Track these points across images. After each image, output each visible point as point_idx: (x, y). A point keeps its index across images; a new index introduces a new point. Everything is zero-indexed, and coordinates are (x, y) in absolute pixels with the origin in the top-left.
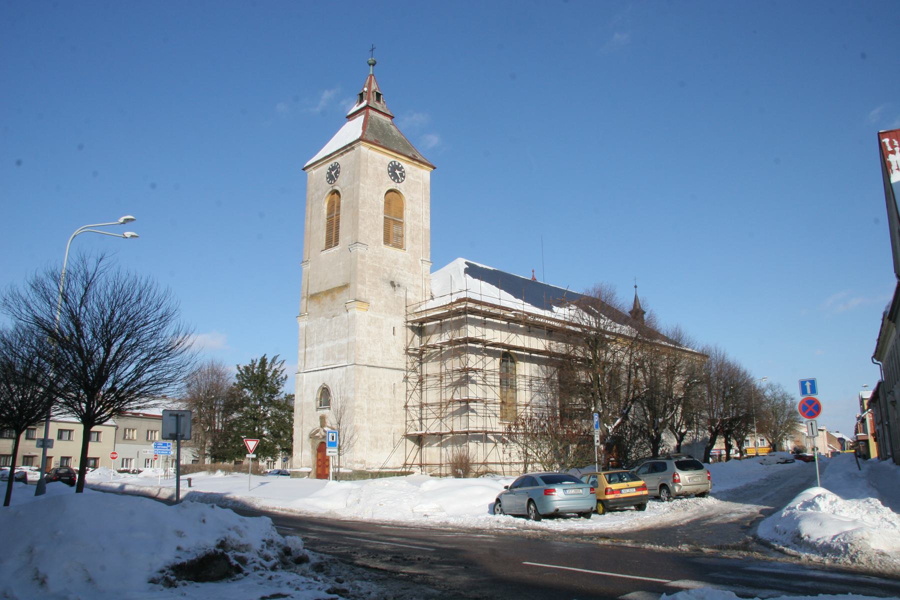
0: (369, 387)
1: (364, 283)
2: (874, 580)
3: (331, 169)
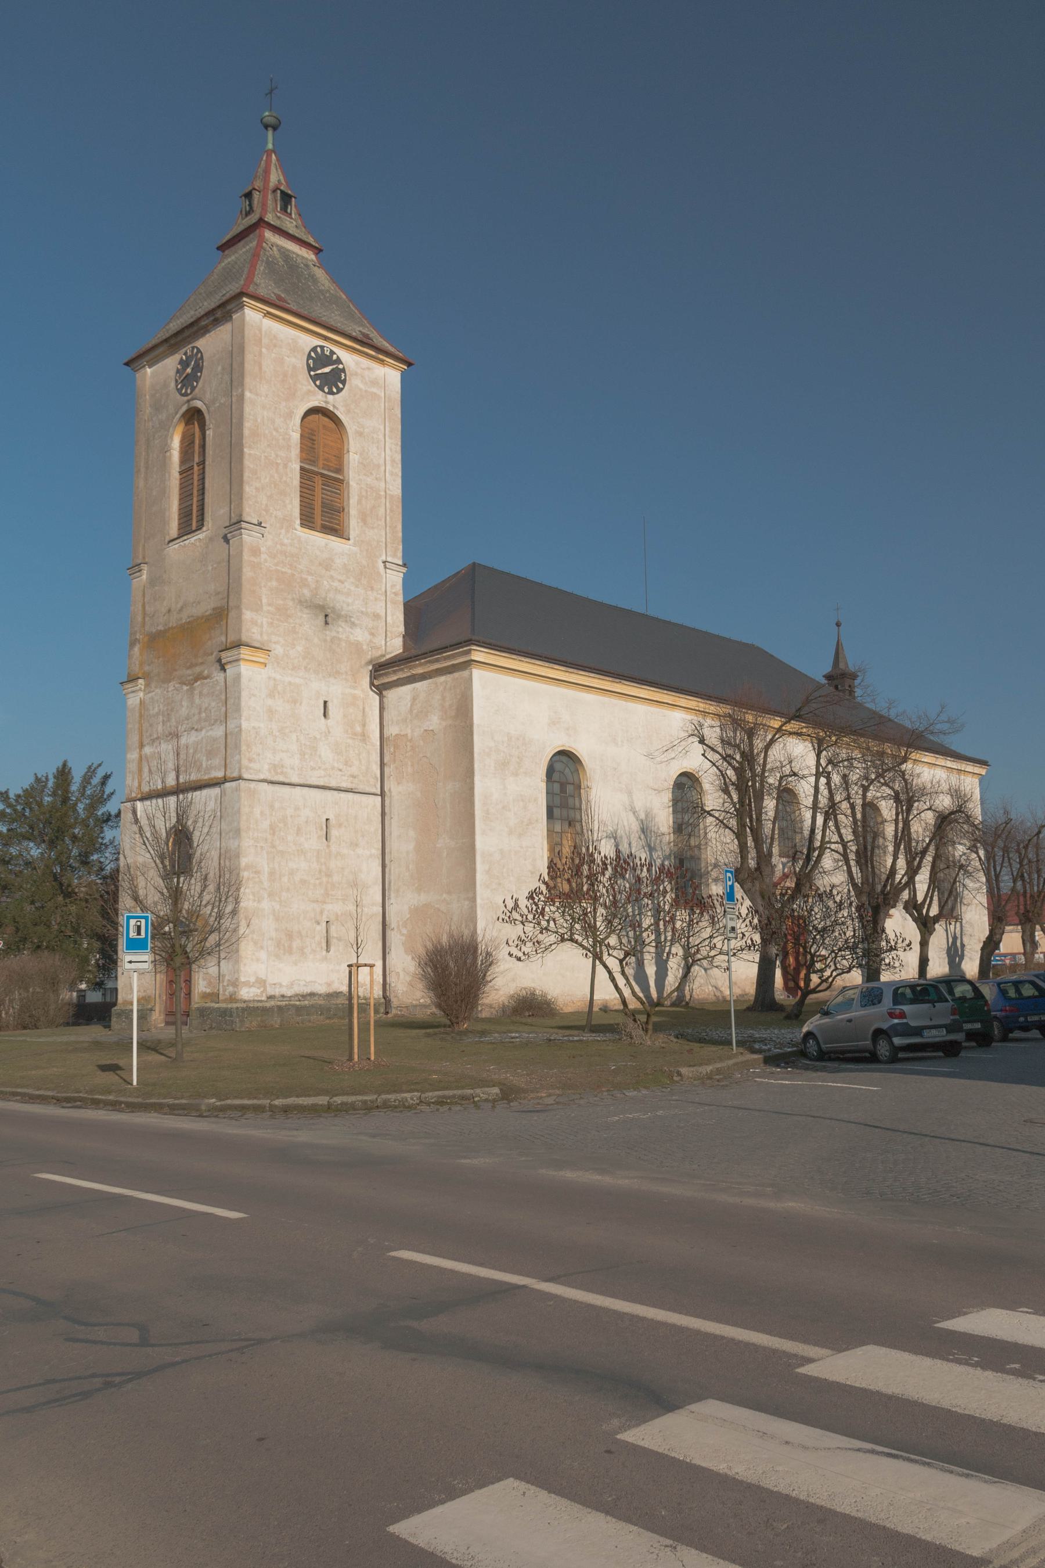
0: (273, 828)
1: (258, 608)
2: (181, 1112)
3: (184, 364)
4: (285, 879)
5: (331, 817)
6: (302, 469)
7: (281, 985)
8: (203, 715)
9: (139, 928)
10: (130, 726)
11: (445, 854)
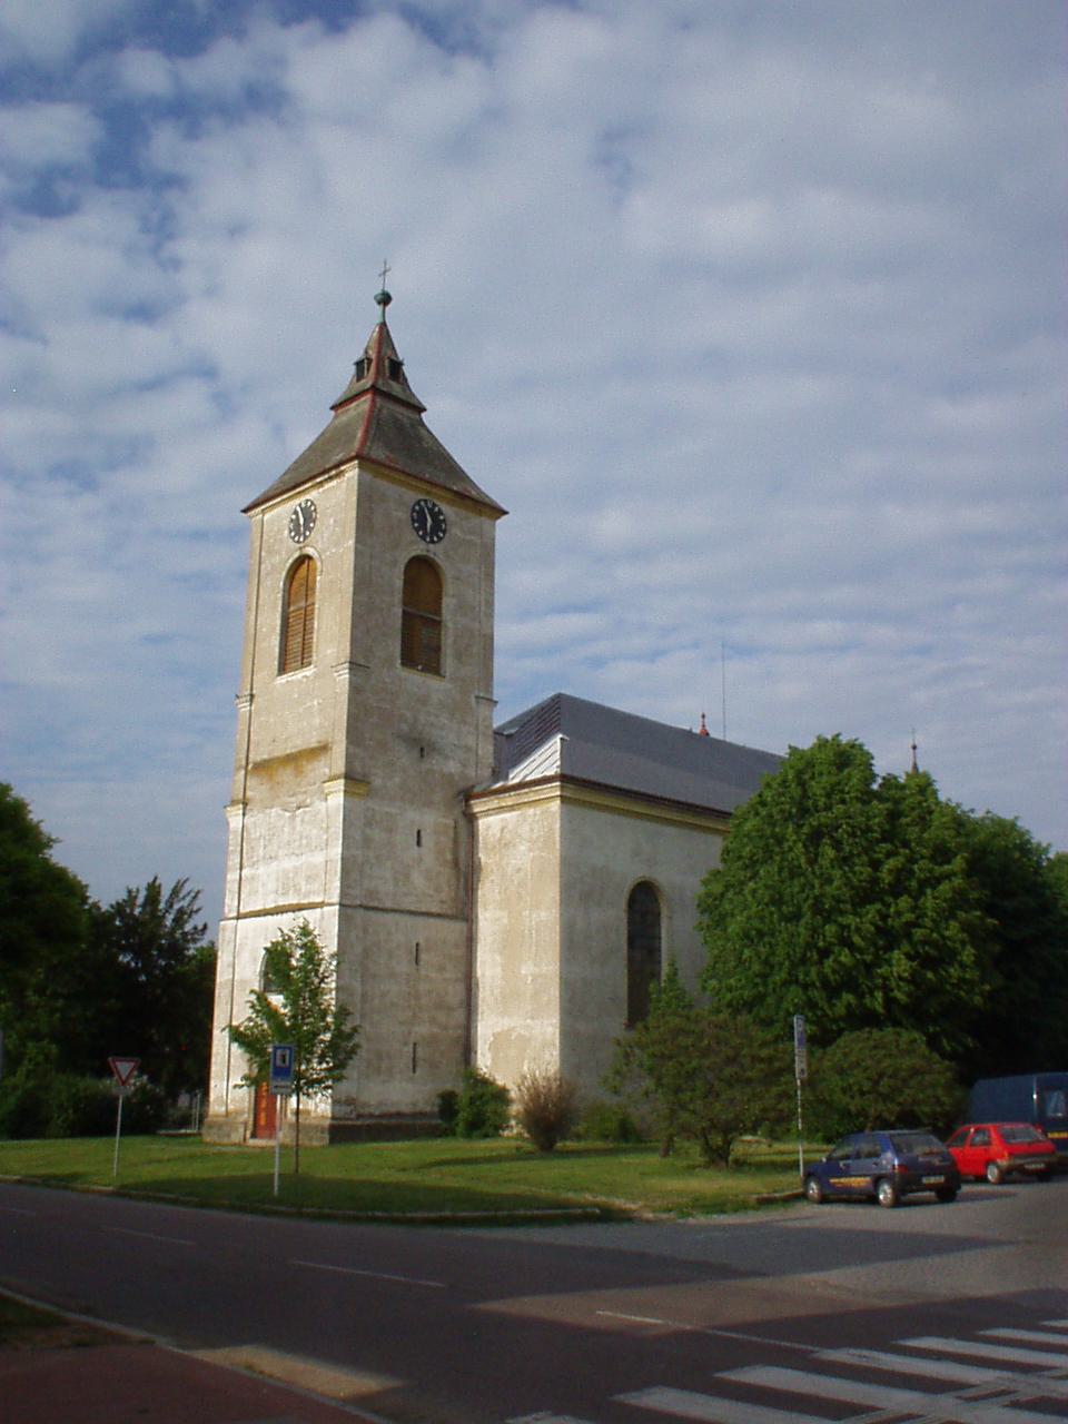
4: (377, 1001)
5: (421, 941)
6: (404, 612)
7: (369, 1106)
8: (304, 842)
9: (284, 1057)
10: (231, 848)
11: (529, 982)
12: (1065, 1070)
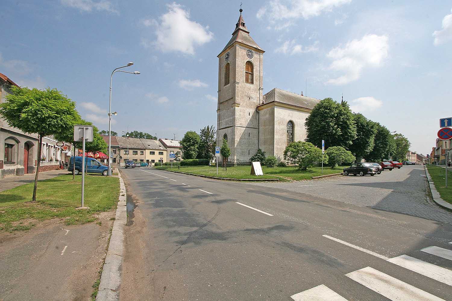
1: (238, 97)
12: (451, 213)
